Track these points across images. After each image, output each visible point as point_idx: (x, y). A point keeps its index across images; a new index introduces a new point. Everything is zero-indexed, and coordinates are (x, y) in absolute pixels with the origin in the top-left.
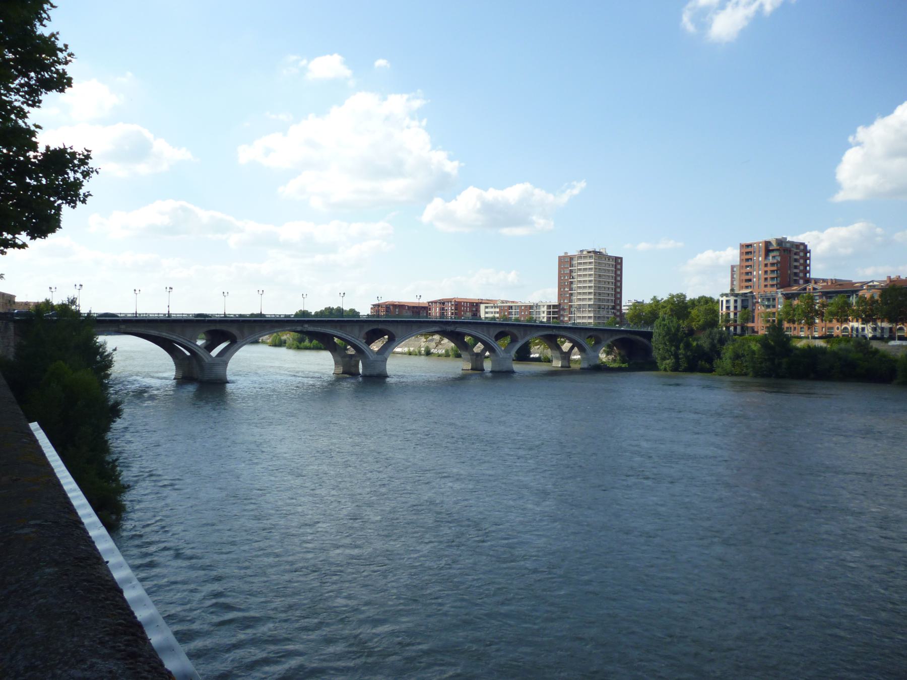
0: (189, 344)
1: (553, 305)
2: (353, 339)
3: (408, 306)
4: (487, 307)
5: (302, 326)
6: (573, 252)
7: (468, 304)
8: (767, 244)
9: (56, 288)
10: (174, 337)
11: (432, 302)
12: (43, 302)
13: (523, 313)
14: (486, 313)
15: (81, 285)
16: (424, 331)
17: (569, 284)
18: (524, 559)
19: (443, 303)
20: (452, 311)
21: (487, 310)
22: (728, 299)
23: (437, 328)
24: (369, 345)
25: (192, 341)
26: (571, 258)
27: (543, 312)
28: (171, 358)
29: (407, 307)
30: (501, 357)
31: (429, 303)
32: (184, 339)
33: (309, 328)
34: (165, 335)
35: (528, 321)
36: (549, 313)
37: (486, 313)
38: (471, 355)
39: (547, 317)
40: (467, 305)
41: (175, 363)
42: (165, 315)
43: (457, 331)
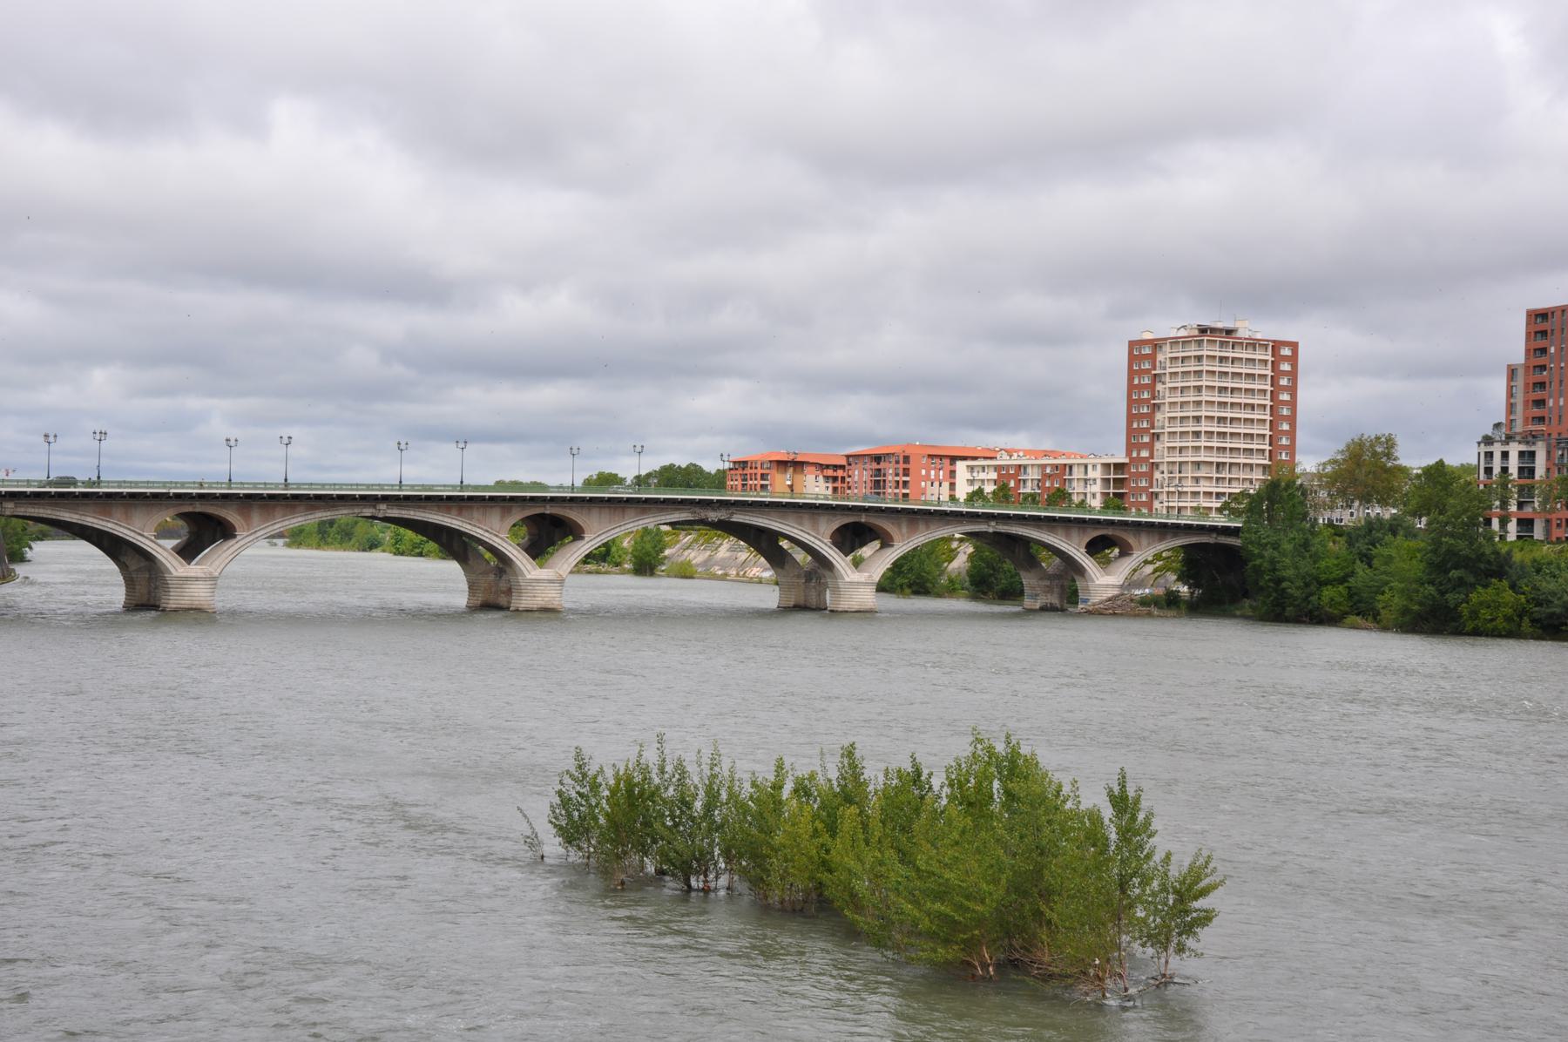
0: (140, 538)
1: (1115, 465)
2: (486, 534)
5: (375, 507)
9: (407, 444)
10: (110, 525)
12: (1457, 467)
15: (290, 438)
16: (652, 520)
18: (885, 993)
23: (683, 515)
28: (462, 571)
32: (129, 529)
33: (389, 511)
43: (733, 522)
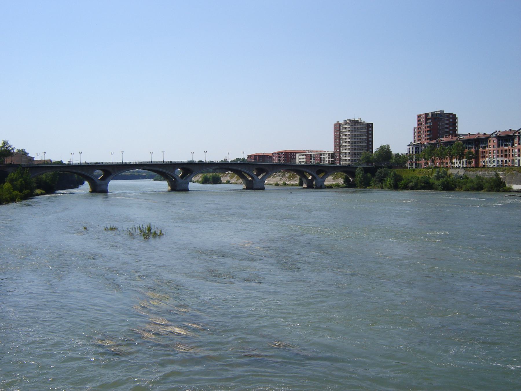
3: (269, 156)
4: (300, 155)
6: (341, 122)
7: (294, 153)
8: (427, 115)
11: (274, 153)
13: (317, 159)
14: (300, 159)
15: (81, 152)
17: (339, 140)
19: (279, 153)
20: (284, 158)
21: (300, 157)
22: (413, 147)
24: (258, 176)
25: (92, 174)
26: (340, 125)
27: (327, 157)
29: (268, 156)
30: (257, 181)
31: (273, 153)
34: (162, 170)
35: (317, 164)
36: (329, 158)
37: (300, 159)
38: (246, 181)
39: (329, 160)
40: (293, 154)
41: (168, 184)
42: (162, 162)
